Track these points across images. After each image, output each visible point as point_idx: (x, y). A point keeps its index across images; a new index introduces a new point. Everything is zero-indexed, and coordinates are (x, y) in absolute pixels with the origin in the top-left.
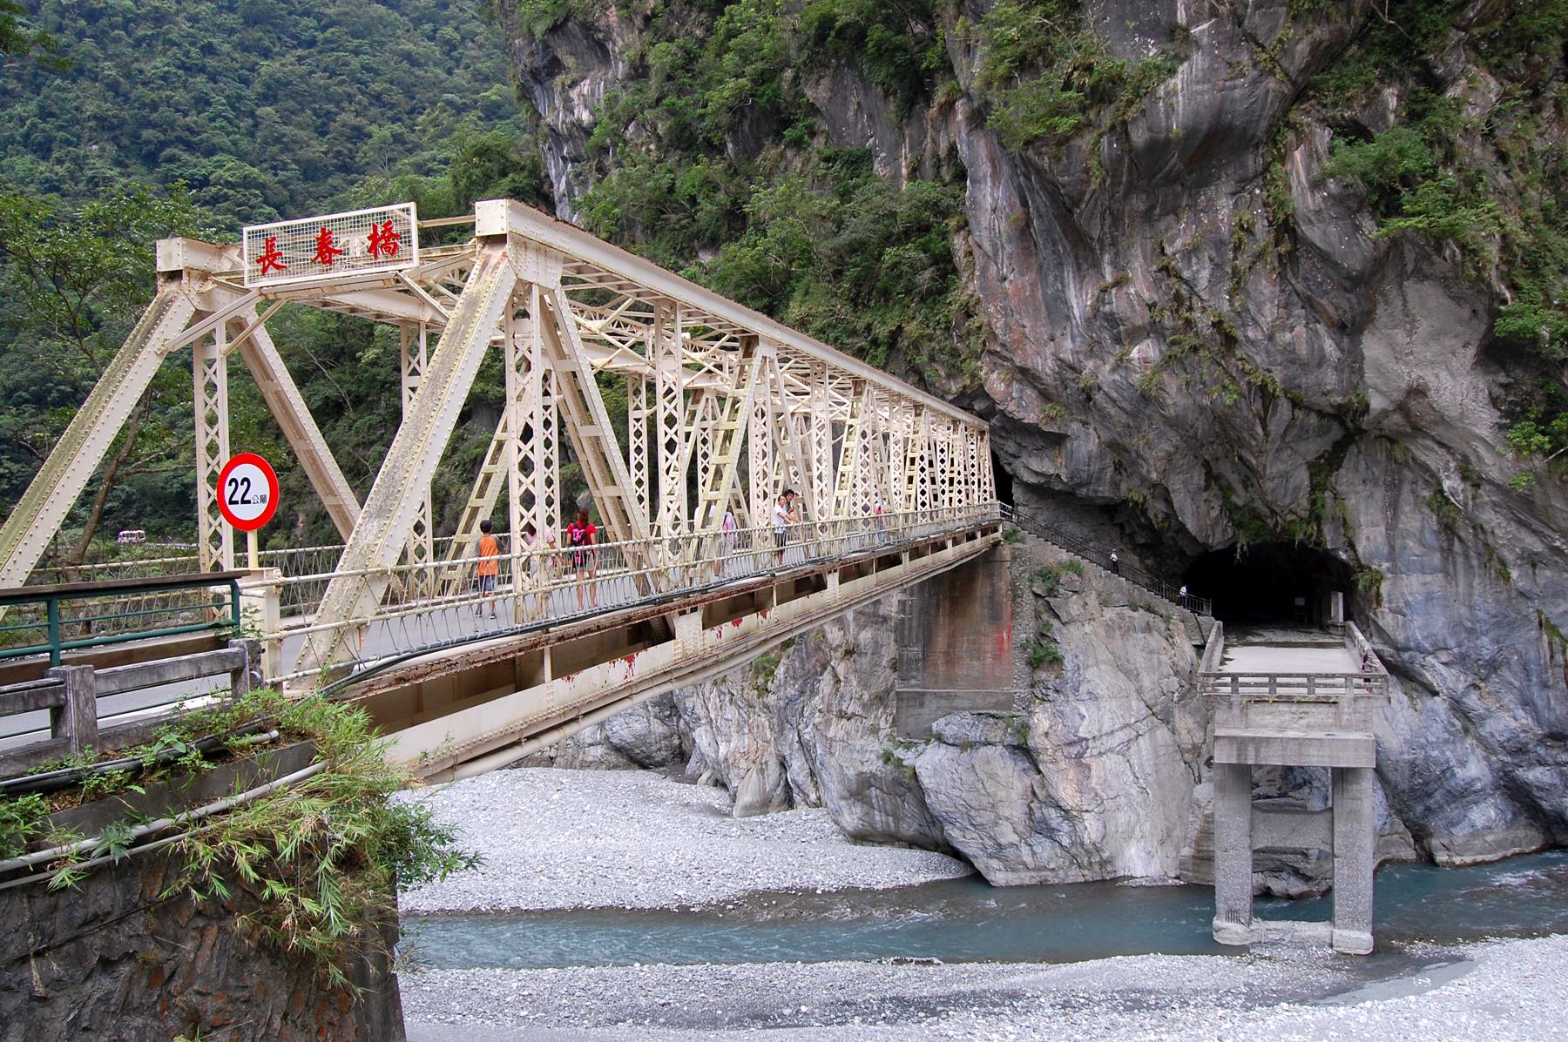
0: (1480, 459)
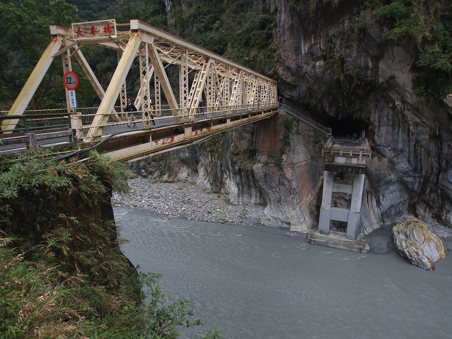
0: (407, 97)
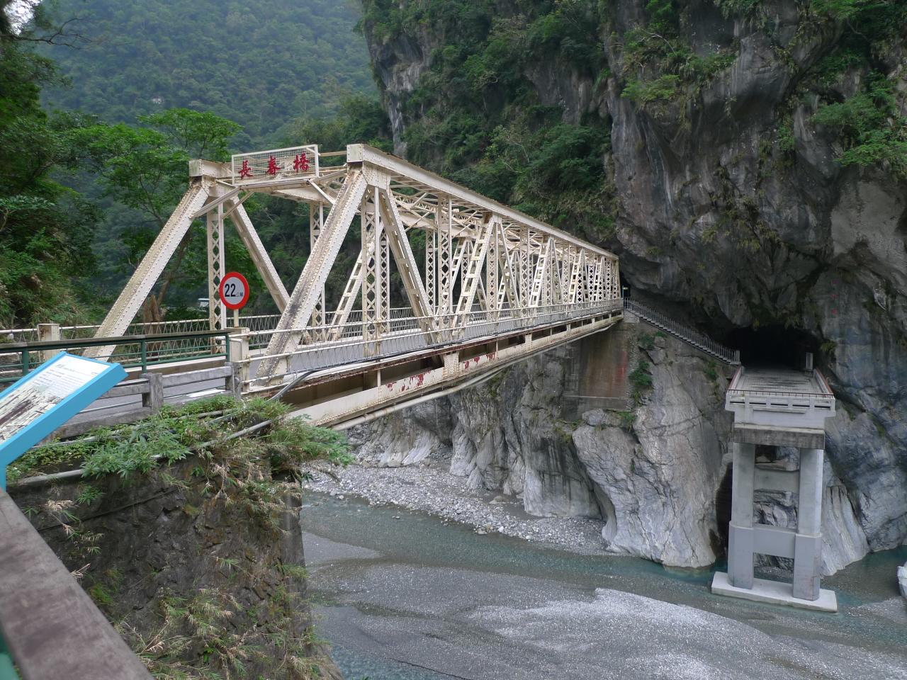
0: (897, 282)
